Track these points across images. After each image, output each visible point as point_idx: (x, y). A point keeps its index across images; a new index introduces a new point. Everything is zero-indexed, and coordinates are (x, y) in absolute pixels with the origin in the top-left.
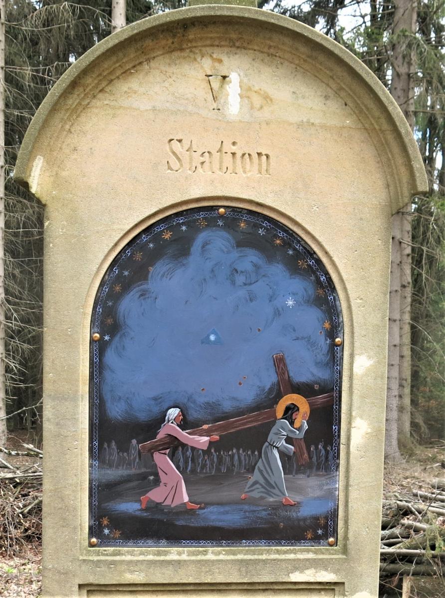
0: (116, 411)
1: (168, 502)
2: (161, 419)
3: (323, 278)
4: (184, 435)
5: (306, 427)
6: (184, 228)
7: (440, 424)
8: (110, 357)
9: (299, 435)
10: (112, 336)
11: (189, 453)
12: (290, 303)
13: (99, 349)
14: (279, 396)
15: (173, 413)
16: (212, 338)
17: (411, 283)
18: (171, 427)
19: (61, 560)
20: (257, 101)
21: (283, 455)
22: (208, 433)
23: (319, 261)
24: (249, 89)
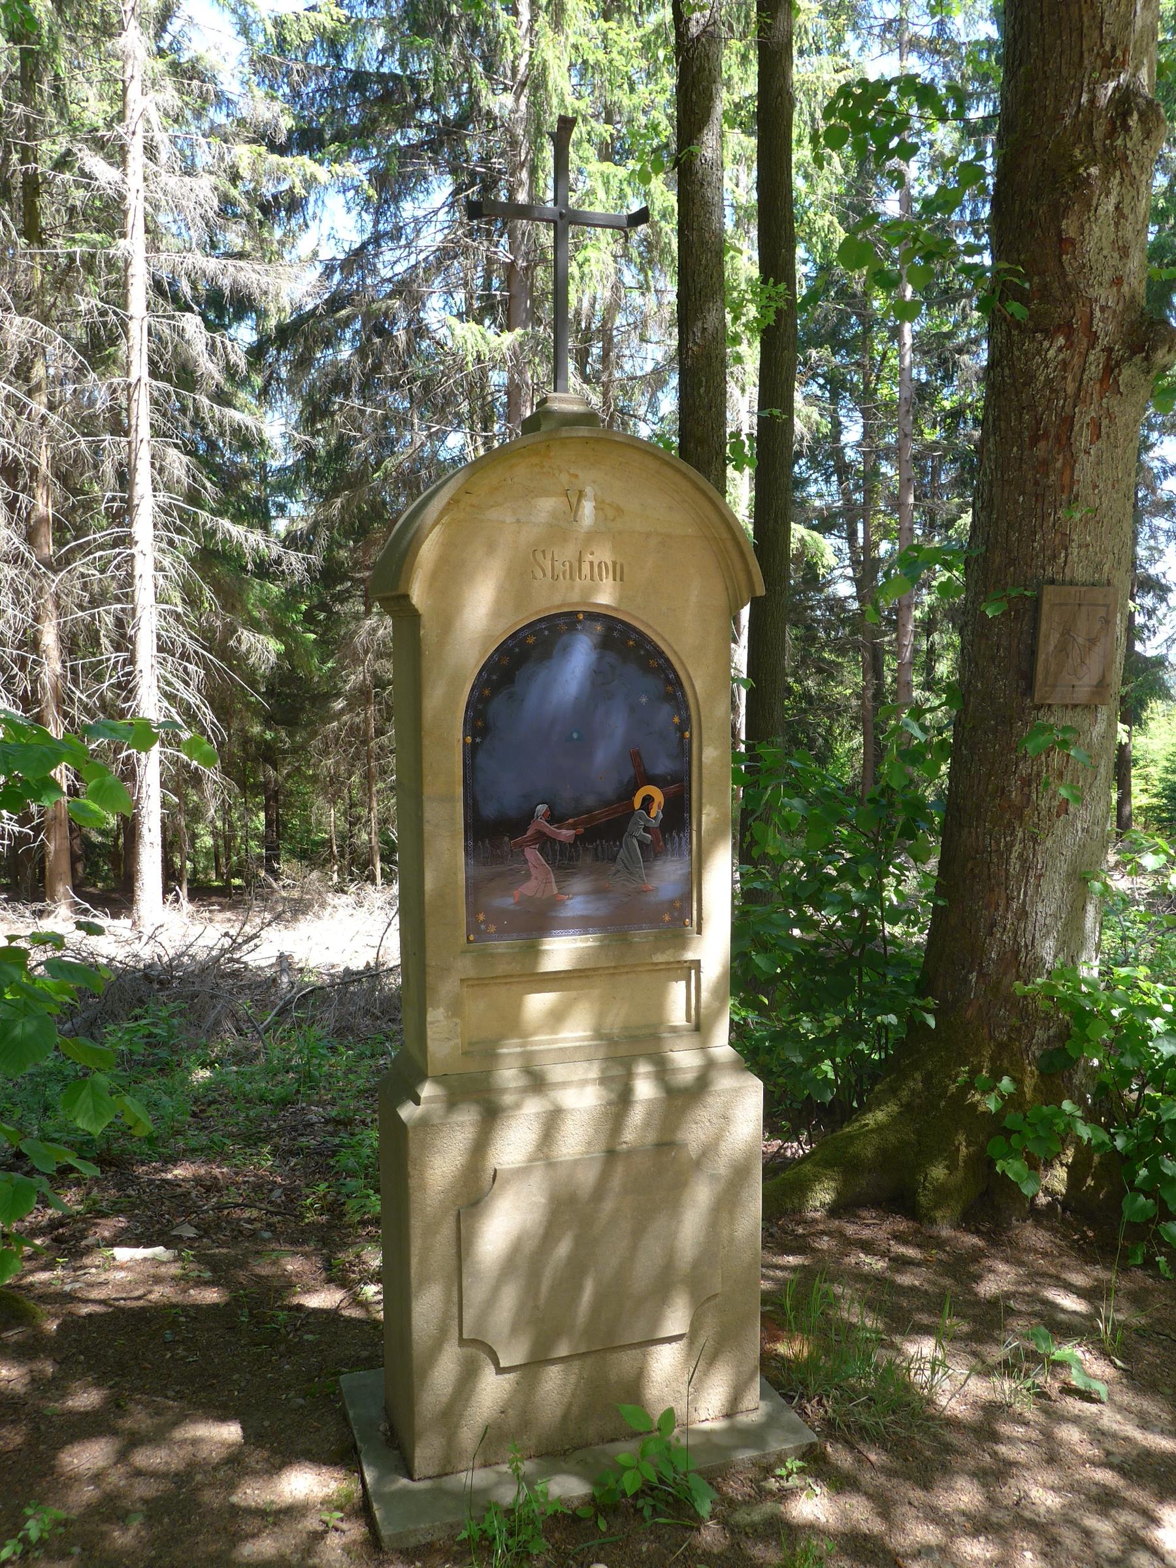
0: (489, 810)
1: (539, 895)
2: (530, 815)
3: (671, 676)
4: (550, 829)
5: (661, 816)
6: (838, 1060)
7: (808, 737)
8: (481, 757)
9: (654, 824)
10: (483, 738)
11: (557, 847)
12: (644, 700)
13: (471, 753)
14: (637, 788)
15: (542, 808)
16: (575, 736)
17: (795, 53)
18: (540, 823)
19: (182, 1013)
20: (610, 513)
21: (641, 844)
22: (573, 826)
23: (667, 660)
24: (603, 502)
